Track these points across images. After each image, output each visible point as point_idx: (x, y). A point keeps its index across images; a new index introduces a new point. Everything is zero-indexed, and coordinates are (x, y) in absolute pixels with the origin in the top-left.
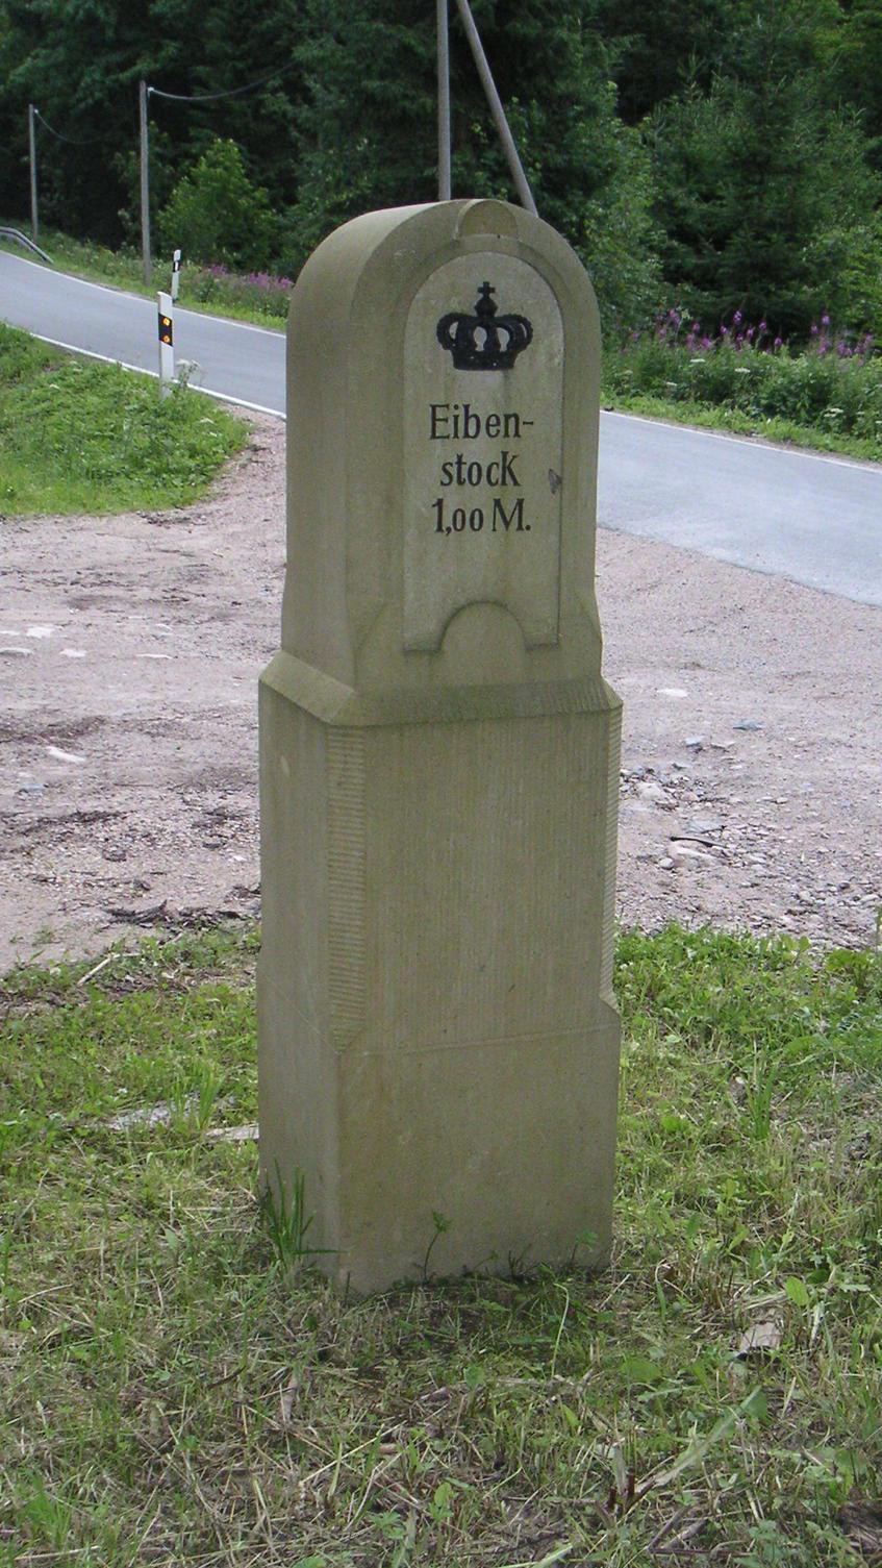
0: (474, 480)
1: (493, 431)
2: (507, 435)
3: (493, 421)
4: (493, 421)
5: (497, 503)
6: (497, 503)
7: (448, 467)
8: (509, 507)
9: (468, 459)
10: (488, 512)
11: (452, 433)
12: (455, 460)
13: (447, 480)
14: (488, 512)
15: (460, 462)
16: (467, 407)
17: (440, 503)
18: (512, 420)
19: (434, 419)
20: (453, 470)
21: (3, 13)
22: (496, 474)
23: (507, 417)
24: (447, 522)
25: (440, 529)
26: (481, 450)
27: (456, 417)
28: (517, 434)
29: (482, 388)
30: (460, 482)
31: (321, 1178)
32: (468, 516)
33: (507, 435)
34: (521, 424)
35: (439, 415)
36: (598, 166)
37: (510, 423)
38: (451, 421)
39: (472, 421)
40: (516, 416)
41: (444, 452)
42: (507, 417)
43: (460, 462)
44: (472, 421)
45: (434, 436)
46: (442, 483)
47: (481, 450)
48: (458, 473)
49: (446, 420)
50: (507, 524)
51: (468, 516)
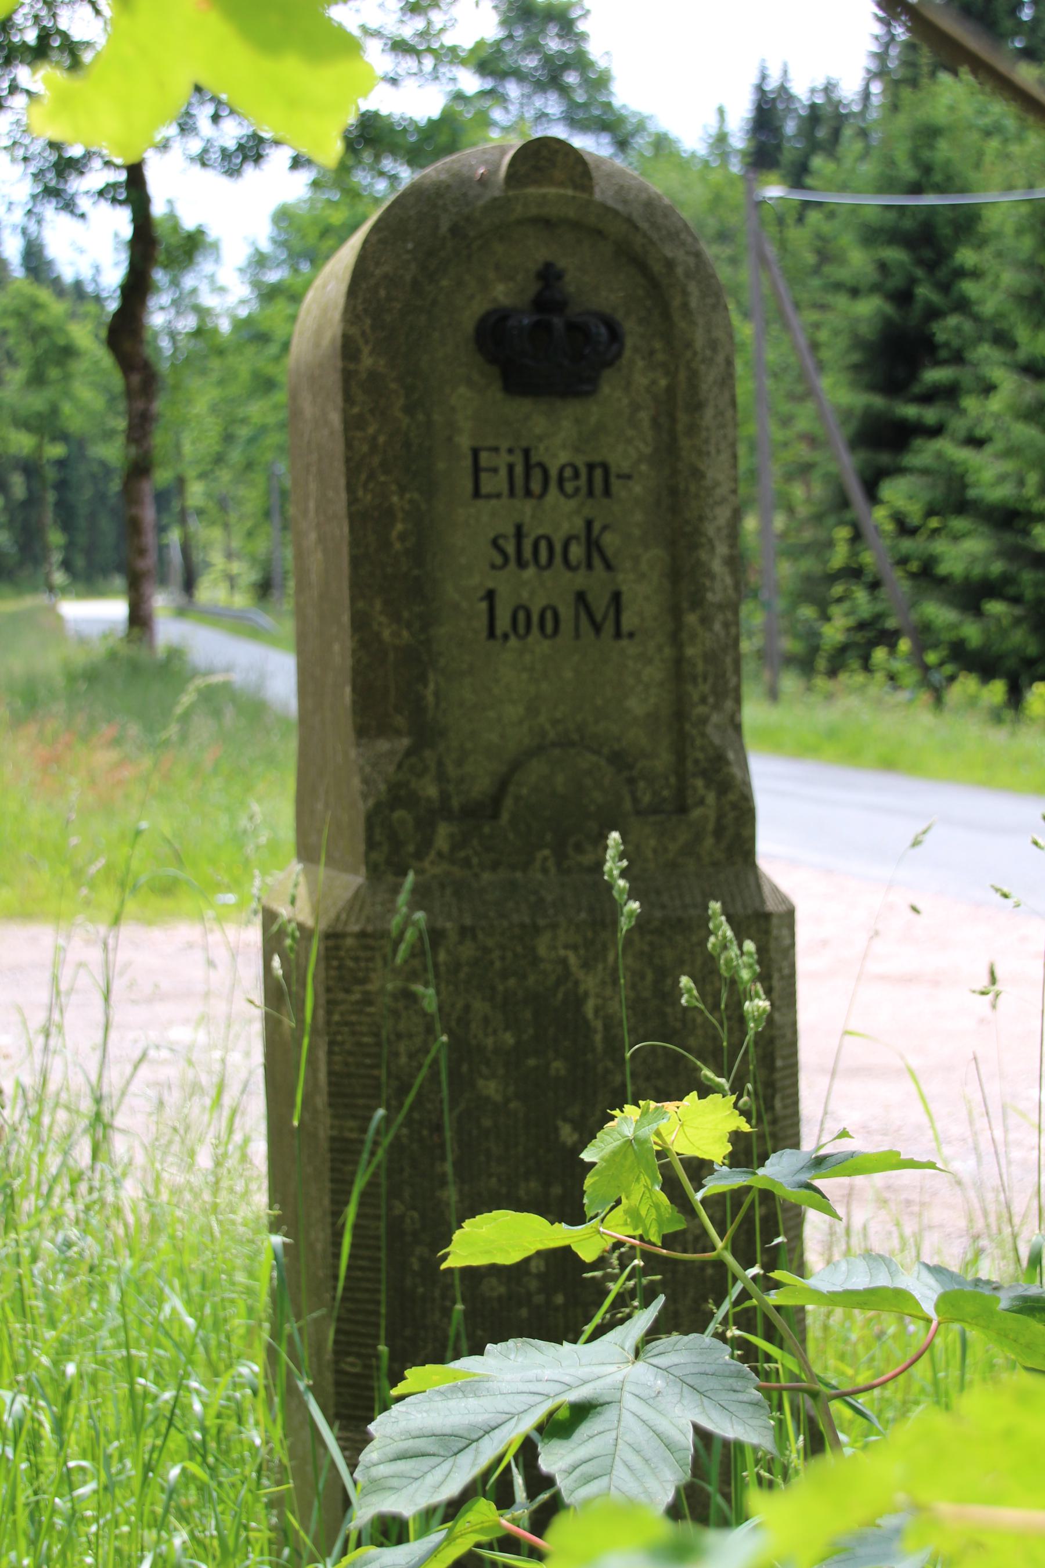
0: (543, 545)
1: (569, 487)
2: (591, 493)
3: (568, 473)
4: (568, 473)
5: (581, 597)
6: (581, 597)
7: (501, 542)
8: (600, 603)
9: (533, 531)
10: (566, 612)
11: (504, 487)
12: (511, 531)
13: (499, 560)
14: (566, 612)
15: (519, 533)
16: (527, 453)
17: (490, 596)
18: (598, 473)
19: (477, 469)
20: (510, 549)
21: (4, 1040)
22: (576, 551)
23: (591, 467)
24: (503, 623)
25: (491, 634)
26: (559, 515)
27: (511, 468)
28: (607, 492)
29: (557, 433)
30: (521, 564)
31: (133, 1001)
32: (535, 618)
33: (591, 493)
34: (613, 480)
35: (484, 458)
36: (840, 600)
37: (597, 479)
38: (503, 472)
39: (537, 475)
40: (605, 467)
41: (493, 517)
42: (591, 467)
43: (519, 533)
44: (537, 475)
45: (477, 493)
46: (493, 567)
47: (559, 515)
48: (518, 550)
49: (495, 470)
50: (597, 628)
51: (535, 618)
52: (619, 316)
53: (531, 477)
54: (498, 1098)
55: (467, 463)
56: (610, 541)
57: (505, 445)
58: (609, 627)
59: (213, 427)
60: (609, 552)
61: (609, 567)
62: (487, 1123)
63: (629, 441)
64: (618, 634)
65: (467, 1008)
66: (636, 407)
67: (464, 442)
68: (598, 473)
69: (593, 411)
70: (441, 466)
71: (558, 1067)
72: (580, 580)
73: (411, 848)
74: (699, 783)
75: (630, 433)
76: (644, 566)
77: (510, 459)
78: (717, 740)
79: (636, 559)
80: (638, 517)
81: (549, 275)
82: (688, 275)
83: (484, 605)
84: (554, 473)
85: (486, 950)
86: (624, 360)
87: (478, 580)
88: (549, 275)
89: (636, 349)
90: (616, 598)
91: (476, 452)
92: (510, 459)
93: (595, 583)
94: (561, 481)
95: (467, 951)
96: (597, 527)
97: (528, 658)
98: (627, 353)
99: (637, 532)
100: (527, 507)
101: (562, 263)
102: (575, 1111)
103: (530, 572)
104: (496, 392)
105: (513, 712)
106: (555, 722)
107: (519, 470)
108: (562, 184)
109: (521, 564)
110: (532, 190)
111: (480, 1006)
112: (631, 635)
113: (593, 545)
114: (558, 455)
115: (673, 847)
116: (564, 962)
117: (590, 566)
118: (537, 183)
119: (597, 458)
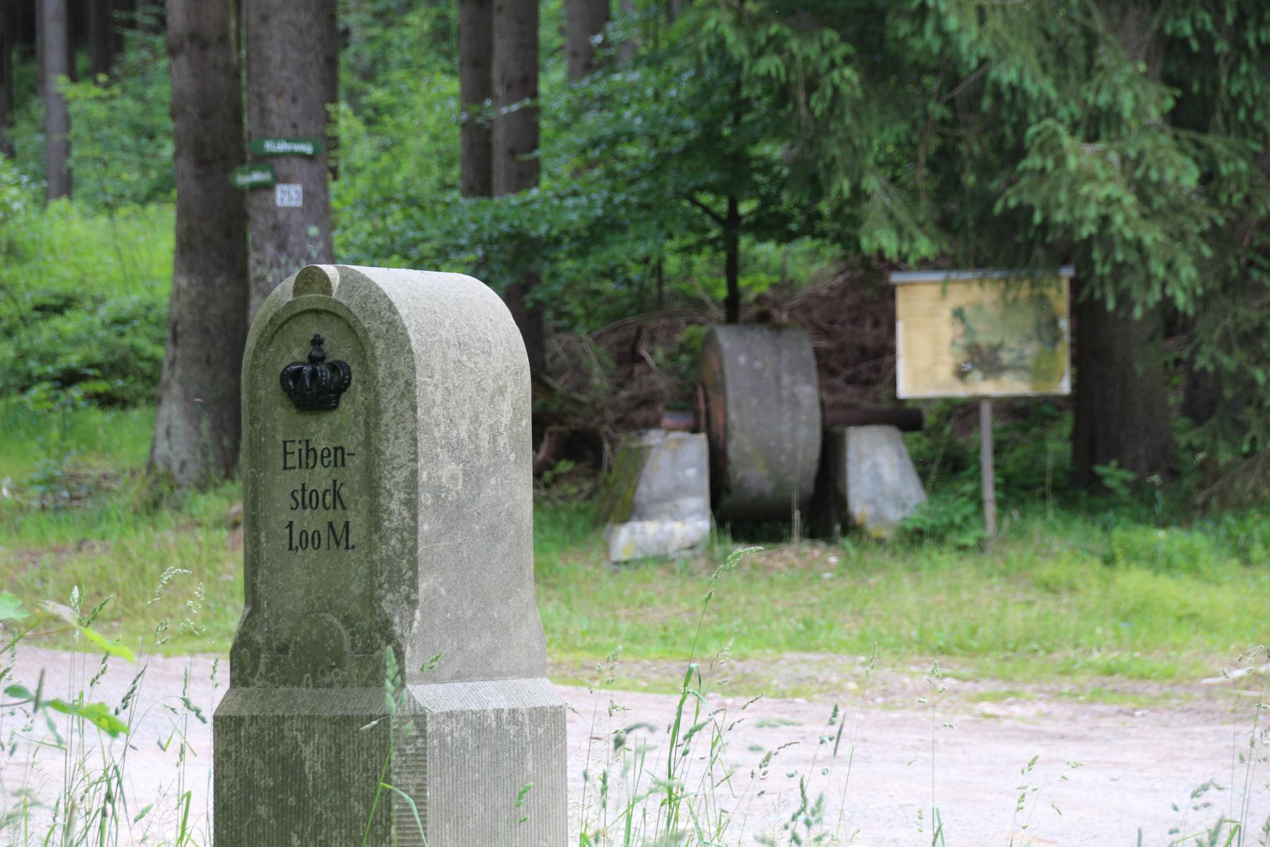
2: (336, 465)
5: (330, 525)
8: (339, 529)
9: (309, 488)
10: (324, 535)
14: (324, 535)
17: (290, 525)
18: (339, 452)
19: (286, 453)
20: (299, 499)
22: (329, 498)
23: (336, 449)
25: (291, 548)
26: (321, 478)
28: (343, 464)
29: (321, 431)
33: (336, 465)
35: (289, 447)
37: (339, 456)
38: (297, 454)
39: (311, 453)
40: (342, 448)
42: (336, 449)
44: (311, 453)
45: (285, 468)
47: (321, 478)
48: (305, 499)
50: (338, 543)
52: (349, 363)
53: (309, 457)
54: (265, 816)
55: (281, 450)
56: (344, 492)
57: (297, 440)
58: (343, 542)
59: (947, 680)
60: (344, 499)
61: (344, 508)
62: (260, 830)
63: (353, 434)
64: (347, 548)
65: (253, 763)
66: (357, 414)
67: (280, 438)
68: (339, 452)
69: (336, 417)
70: (270, 452)
71: (292, 801)
72: (330, 515)
73: (249, 671)
74: (378, 636)
75: (354, 429)
76: (360, 507)
77: (300, 446)
78: (388, 611)
79: (356, 502)
80: (357, 478)
81: (317, 342)
82: (377, 337)
83: (287, 530)
84: (319, 454)
85: (262, 730)
86: (352, 387)
87: (286, 516)
88: (317, 342)
89: (357, 381)
90: (347, 524)
91: (285, 443)
92: (300, 446)
93: (334, 516)
94: (322, 457)
95: (254, 730)
96: (338, 483)
97: (306, 561)
98: (353, 383)
99: (357, 487)
100: (306, 474)
101: (323, 335)
102: (299, 827)
103: (309, 510)
104: (293, 411)
105: (300, 592)
106: (319, 598)
107: (304, 452)
108: (317, 292)
109: (304, 508)
110: (305, 296)
111: (259, 763)
112: (353, 547)
113: (336, 494)
114: (320, 444)
115: (366, 674)
116: (295, 738)
117: (335, 507)
118: (307, 292)
119: (337, 444)
